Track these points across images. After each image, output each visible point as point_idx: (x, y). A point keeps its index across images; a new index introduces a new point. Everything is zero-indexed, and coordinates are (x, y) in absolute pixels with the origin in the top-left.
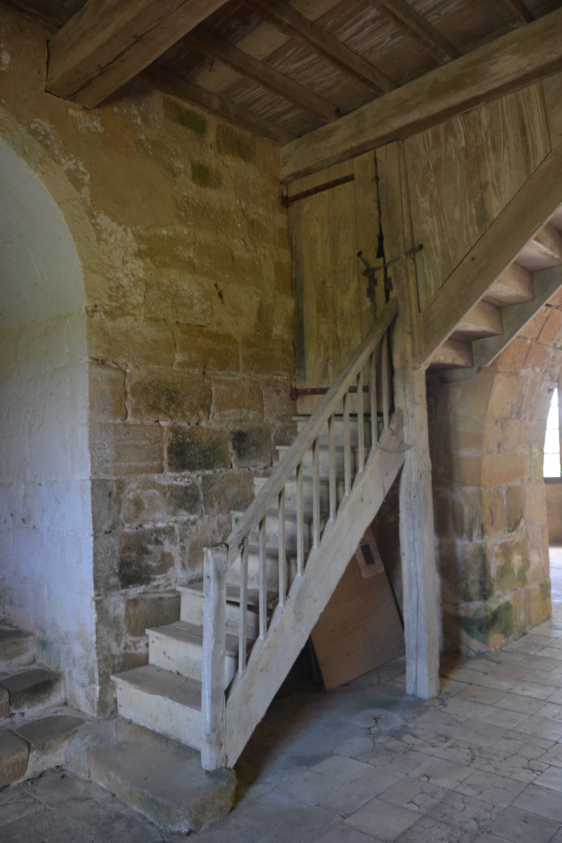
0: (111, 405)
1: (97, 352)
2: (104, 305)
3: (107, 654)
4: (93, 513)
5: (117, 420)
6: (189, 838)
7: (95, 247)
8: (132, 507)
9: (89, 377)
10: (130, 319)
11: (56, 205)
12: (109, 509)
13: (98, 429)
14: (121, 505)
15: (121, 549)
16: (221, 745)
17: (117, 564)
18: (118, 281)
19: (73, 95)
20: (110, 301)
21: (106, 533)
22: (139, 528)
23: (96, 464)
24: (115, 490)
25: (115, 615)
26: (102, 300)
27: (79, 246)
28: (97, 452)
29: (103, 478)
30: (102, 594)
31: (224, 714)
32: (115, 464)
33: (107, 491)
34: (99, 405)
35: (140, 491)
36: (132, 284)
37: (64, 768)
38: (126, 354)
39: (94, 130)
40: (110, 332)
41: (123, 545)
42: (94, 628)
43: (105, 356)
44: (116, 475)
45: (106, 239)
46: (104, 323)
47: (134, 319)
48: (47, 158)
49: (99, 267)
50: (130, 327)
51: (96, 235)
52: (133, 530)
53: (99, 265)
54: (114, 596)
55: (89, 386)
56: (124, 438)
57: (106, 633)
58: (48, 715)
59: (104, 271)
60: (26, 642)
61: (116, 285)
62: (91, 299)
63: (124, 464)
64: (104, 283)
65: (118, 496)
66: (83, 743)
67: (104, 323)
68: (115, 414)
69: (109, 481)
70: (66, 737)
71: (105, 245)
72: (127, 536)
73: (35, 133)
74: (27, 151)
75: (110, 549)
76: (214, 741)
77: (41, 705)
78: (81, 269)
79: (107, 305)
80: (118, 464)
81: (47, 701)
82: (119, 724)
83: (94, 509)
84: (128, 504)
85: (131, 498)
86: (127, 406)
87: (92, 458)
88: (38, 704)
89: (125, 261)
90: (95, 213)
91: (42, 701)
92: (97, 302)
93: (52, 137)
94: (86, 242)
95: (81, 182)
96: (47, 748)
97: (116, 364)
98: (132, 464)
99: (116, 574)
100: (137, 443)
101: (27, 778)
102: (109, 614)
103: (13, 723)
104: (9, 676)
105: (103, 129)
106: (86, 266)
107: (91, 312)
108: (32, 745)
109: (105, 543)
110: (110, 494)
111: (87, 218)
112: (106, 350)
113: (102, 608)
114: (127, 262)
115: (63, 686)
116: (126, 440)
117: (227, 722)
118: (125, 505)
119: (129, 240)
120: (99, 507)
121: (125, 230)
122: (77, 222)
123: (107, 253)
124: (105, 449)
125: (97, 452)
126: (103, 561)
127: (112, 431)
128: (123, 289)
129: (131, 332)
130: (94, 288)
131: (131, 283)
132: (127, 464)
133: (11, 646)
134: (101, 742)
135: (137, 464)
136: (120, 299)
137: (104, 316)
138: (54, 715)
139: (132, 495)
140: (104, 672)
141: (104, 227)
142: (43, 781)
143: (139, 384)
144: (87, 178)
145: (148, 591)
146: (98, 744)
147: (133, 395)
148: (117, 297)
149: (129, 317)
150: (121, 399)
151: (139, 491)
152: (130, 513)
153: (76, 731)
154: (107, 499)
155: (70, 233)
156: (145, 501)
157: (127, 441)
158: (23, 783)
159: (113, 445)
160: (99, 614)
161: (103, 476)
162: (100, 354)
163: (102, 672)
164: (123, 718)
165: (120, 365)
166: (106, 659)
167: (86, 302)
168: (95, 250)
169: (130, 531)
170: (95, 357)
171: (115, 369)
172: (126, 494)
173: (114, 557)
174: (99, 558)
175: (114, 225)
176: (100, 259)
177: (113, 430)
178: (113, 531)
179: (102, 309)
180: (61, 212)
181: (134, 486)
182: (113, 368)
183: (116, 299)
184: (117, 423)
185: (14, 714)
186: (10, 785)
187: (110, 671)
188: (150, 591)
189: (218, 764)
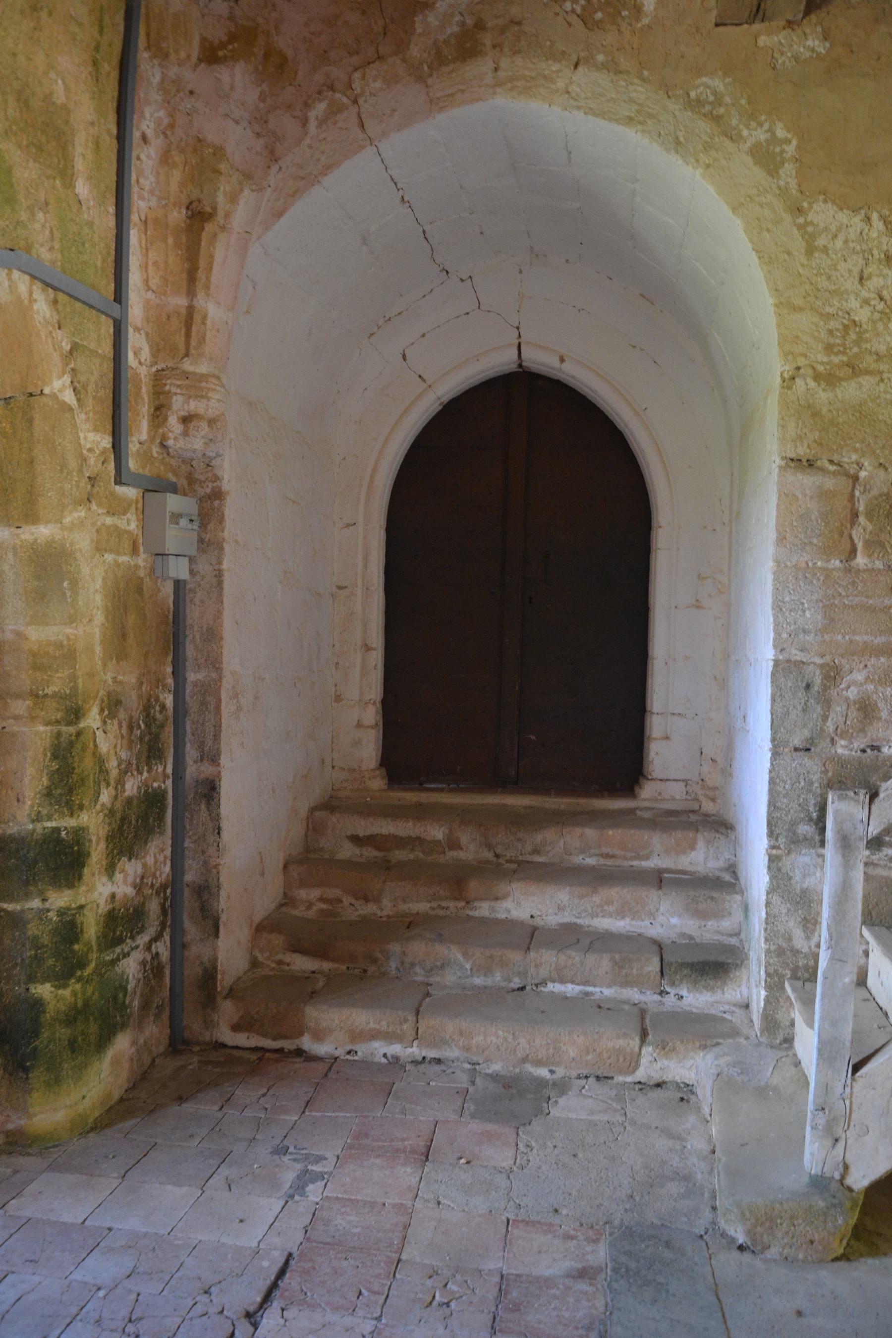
0: (820, 535)
1: (796, 447)
2: (815, 365)
3: (784, 945)
4: (772, 714)
5: (832, 561)
6: (736, 1254)
7: (803, 265)
8: (853, 714)
9: (779, 491)
10: (867, 381)
11: (729, 212)
12: (804, 710)
13: (790, 577)
14: (829, 707)
15: (825, 782)
16: (837, 1140)
17: (815, 805)
18: (847, 316)
19: (758, 10)
20: (829, 355)
21: (796, 749)
22: (869, 751)
23: (785, 636)
24: (818, 680)
25: (805, 886)
26: (812, 356)
27: (769, 271)
28: (787, 614)
29: (798, 658)
30: (782, 846)
31: (848, 1090)
32: (823, 637)
33: (802, 681)
34: (796, 537)
35: (872, 687)
36: (877, 316)
37: (695, 1090)
38: (858, 445)
39: (808, 54)
40: (825, 410)
41: (830, 774)
42: (764, 897)
43: (813, 452)
44: (822, 656)
45: (825, 247)
46: (812, 395)
47: (878, 379)
48: (717, 139)
49: (809, 299)
50: (869, 396)
51: (804, 244)
52: (854, 753)
53: (809, 295)
54: (805, 855)
55: (778, 505)
56: (844, 593)
57: (784, 911)
58: (713, 1012)
59: (819, 303)
60: (730, 902)
61: (842, 323)
62: (790, 357)
63: (839, 637)
64: (816, 326)
65: (825, 690)
66: (716, 1062)
67: (812, 395)
68: (827, 552)
69: (809, 664)
70: (700, 1046)
71: (824, 256)
72: (841, 762)
73: (695, 105)
74: (682, 139)
75: (802, 776)
76: (820, 1127)
77: (709, 994)
78: (772, 309)
79: (822, 363)
80: (827, 637)
81: (719, 991)
82: (783, 1059)
83: (775, 708)
84: (844, 707)
85: (851, 697)
86: (855, 537)
87: (777, 625)
88: (705, 992)
89: (865, 276)
90: (805, 205)
91: (712, 989)
92: (801, 362)
93: (728, 100)
94: (785, 261)
95: (779, 159)
96: (670, 1050)
97: (839, 465)
98: (858, 638)
99: (811, 819)
100: (871, 602)
101: (637, 1080)
102: (793, 882)
103: (661, 1003)
104: (693, 942)
105: (827, 45)
106: (781, 303)
107: (789, 381)
108: (650, 1037)
109: (793, 765)
110: (808, 686)
111: (787, 217)
112: (815, 441)
113: (779, 870)
114: (870, 277)
115: (745, 978)
116: (848, 596)
117: (855, 1107)
118: (838, 709)
119: (875, 235)
120: (784, 706)
121: (868, 219)
122: (768, 231)
123: (827, 270)
124: (804, 611)
125: (787, 614)
126: (787, 794)
127: (819, 579)
128: (857, 329)
129: (870, 404)
130: (797, 337)
131: (876, 314)
132: (847, 637)
133: (706, 900)
134: (742, 1073)
135: (866, 638)
136: (851, 349)
137: (812, 384)
138: (720, 1014)
139: (856, 692)
140: (776, 971)
141: (822, 226)
142: (658, 1093)
143: (884, 498)
144: (791, 149)
145: (875, 862)
146: (736, 1074)
147: (869, 516)
148: (844, 345)
149: (867, 377)
150: (842, 525)
151: (870, 687)
152: (848, 722)
153: (718, 1044)
154: (801, 694)
155: (754, 253)
156: (881, 705)
157: (851, 598)
158: (630, 1083)
159: (821, 604)
160: (773, 878)
161: (798, 656)
162: (802, 451)
163: (771, 971)
164: (795, 1055)
165: (846, 466)
166: (780, 952)
167: (779, 365)
168: (801, 271)
169: (846, 752)
170: (793, 455)
171: (834, 473)
172: (843, 690)
173: (809, 791)
174: (780, 789)
175: (843, 217)
176: (811, 284)
177: (822, 578)
178: (813, 749)
179: (810, 372)
180: (738, 222)
181: (859, 676)
182: (828, 472)
183: (842, 349)
184: (830, 566)
185: (668, 993)
186: (612, 1078)
187: (788, 973)
188: (882, 863)
189: (825, 1170)
